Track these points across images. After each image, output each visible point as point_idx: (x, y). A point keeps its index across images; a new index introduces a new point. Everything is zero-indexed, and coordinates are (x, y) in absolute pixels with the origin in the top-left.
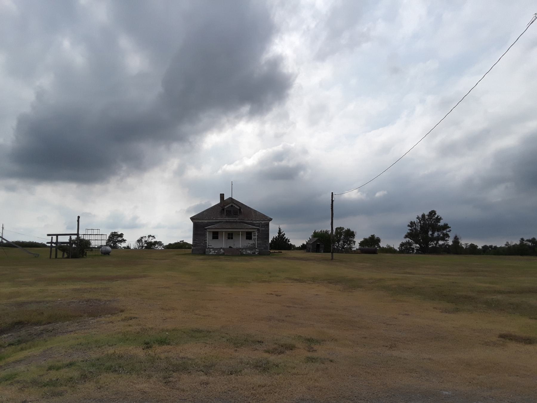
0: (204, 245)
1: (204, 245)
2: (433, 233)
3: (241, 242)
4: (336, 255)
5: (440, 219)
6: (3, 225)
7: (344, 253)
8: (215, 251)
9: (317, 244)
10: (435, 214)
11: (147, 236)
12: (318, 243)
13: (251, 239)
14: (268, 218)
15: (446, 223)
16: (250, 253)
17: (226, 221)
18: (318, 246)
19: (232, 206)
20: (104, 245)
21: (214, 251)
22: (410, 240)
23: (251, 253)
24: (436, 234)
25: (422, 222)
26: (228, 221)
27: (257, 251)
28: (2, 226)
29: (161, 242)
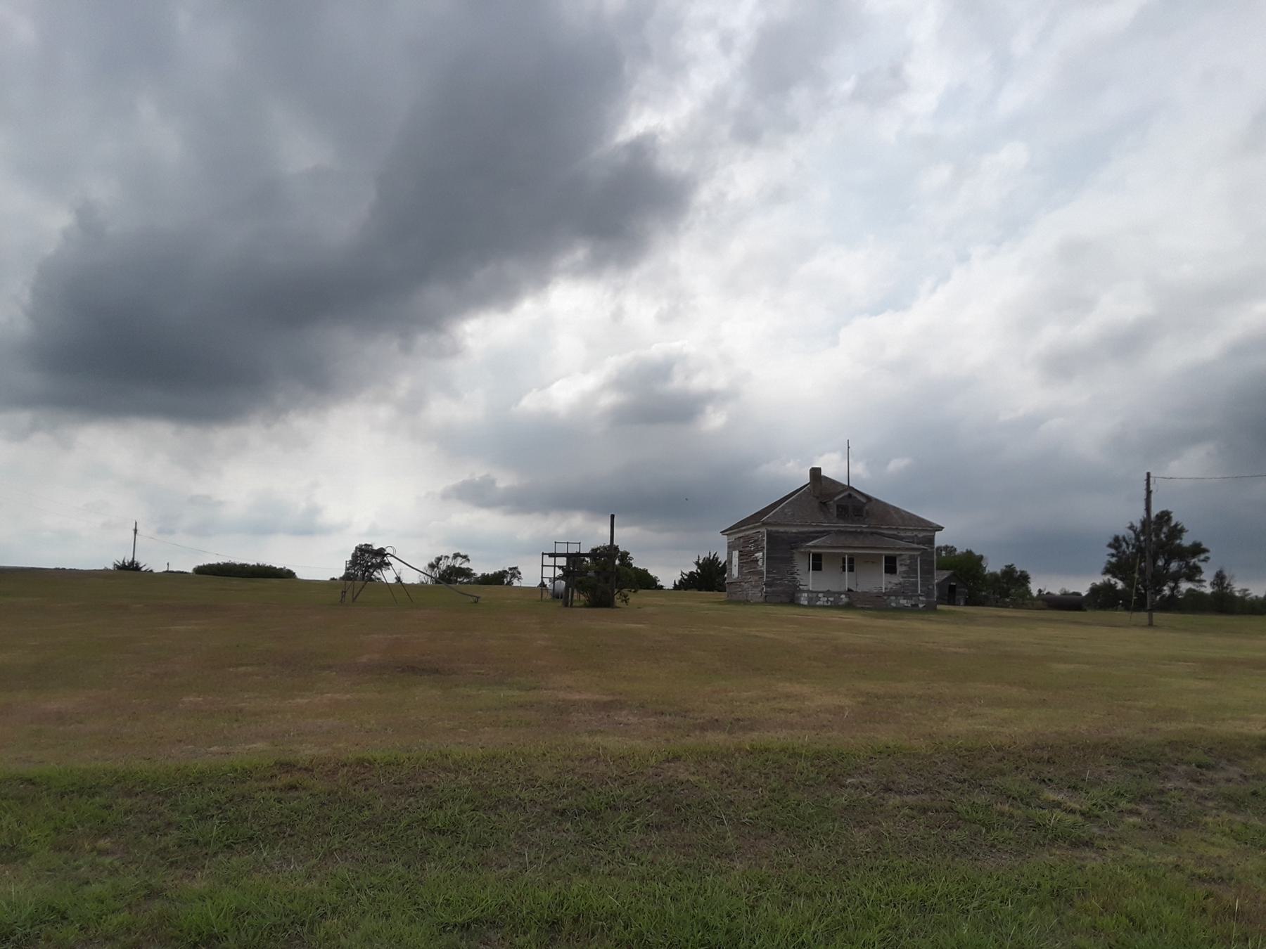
0: (790, 584)
1: (790, 584)
2: (1168, 562)
3: (848, 579)
4: (1157, 616)
5: (1182, 531)
6: (136, 523)
7: (1011, 606)
8: (830, 599)
9: (951, 586)
10: (1169, 519)
11: (451, 556)
12: (952, 584)
13: (895, 572)
14: (934, 526)
15: (1198, 542)
16: (906, 605)
17: (838, 531)
18: (952, 589)
19: (850, 495)
20: (375, 573)
21: (826, 599)
22: (1111, 579)
23: (909, 605)
24: (1174, 566)
25: (1142, 538)
26: (842, 529)
27: (923, 601)
28: (134, 527)
29: (471, 570)
